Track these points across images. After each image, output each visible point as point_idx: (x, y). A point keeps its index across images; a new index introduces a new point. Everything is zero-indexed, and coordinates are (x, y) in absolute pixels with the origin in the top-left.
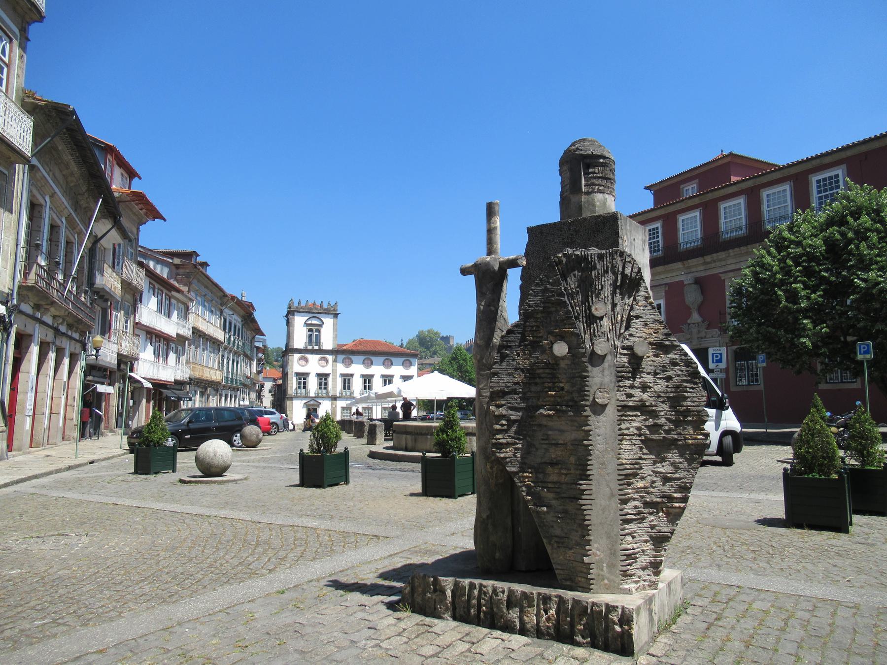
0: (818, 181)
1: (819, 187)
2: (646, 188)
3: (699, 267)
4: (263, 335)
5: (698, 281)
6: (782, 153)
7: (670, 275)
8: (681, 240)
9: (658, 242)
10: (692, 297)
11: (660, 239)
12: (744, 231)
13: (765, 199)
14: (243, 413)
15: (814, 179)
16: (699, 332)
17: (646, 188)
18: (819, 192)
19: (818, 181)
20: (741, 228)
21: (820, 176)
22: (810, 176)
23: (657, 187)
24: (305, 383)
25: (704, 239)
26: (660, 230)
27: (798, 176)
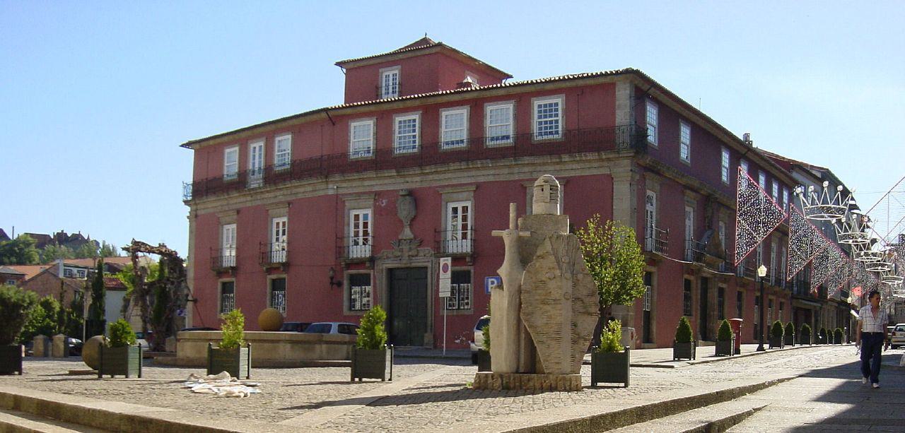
0: (400, 122)
1: (540, 112)
2: (338, 64)
3: (414, 180)
4: (511, 77)
5: (411, 193)
6: (521, 72)
7: (381, 182)
8: (396, 145)
9: (557, 121)
10: (405, 210)
11: (560, 118)
12: (511, 141)
13: (444, 119)
14: (771, 346)
15: (537, 103)
16: (410, 249)
17: (338, 64)
18: (540, 117)
19: (400, 122)
20: (462, 141)
21: (543, 102)
22: (485, 104)
23: (351, 66)
24: (351, 302)
25: (377, 151)
26: (560, 107)
27: (524, 94)
